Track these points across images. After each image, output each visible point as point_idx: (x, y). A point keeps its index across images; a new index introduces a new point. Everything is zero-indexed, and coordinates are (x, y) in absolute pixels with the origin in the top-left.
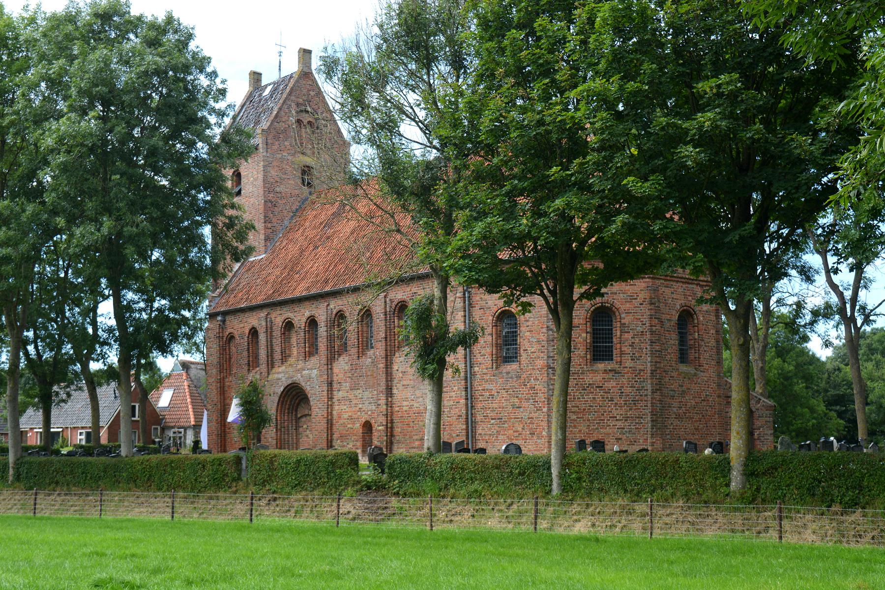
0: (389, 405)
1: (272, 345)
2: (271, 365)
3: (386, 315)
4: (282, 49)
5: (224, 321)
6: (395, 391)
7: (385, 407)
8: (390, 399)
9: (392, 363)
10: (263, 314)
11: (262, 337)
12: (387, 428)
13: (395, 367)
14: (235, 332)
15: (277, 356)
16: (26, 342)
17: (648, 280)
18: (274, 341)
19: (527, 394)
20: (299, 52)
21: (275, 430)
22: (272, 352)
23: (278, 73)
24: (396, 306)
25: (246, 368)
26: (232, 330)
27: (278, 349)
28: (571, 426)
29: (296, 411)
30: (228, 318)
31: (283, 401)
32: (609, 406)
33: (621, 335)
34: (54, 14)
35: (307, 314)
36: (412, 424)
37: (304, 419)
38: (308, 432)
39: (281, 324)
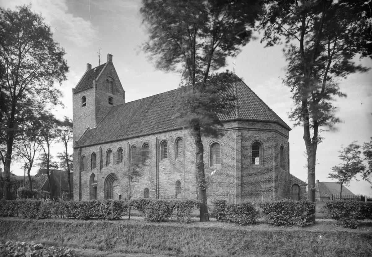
0: (158, 181)
1: (102, 159)
2: (101, 167)
3: (156, 146)
4: (100, 55)
5: (81, 150)
6: (160, 176)
7: (156, 182)
8: (158, 179)
9: (158, 165)
10: (99, 147)
11: (98, 156)
12: (157, 191)
13: (160, 167)
14: (85, 154)
15: (104, 163)
16: (41, 42)
17: (274, 132)
18: (103, 157)
19: (225, 177)
20: (108, 55)
21: (103, 191)
22: (102, 162)
23: (99, 63)
24: (161, 142)
25: (91, 168)
26: (84, 154)
27: (104, 160)
28: (244, 190)
29: (112, 185)
30: (83, 149)
31: (107, 180)
32: (259, 182)
33: (263, 154)
34: (14, 12)
35: (118, 147)
36: (168, 189)
37: (115, 187)
38: (117, 192)
39: (106, 151)
